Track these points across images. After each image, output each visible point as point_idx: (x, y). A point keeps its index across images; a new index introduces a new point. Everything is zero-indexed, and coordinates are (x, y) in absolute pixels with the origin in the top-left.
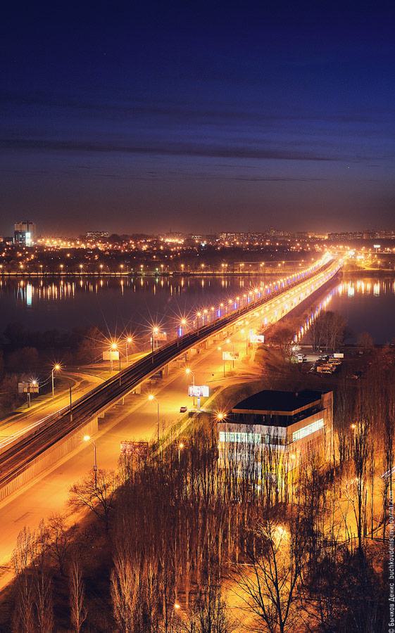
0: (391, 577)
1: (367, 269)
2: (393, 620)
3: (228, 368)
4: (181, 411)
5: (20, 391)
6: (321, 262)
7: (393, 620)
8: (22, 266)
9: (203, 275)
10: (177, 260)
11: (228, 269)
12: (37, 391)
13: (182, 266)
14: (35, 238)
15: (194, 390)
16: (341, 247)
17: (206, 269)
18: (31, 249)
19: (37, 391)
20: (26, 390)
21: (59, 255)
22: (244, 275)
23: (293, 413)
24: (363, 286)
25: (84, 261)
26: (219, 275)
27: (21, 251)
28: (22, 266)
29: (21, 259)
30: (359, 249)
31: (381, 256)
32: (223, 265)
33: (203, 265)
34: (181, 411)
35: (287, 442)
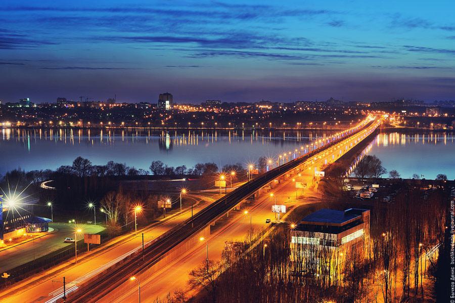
0: (452, 263)
1: (397, 127)
2: (453, 294)
3: (299, 193)
4: (267, 222)
5: (159, 207)
6: (364, 123)
7: (453, 294)
8: (163, 123)
9: (284, 130)
10: (267, 120)
11: (301, 126)
12: (170, 206)
13: (270, 124)
14: (172, 104)
15: (275, 208)
16: (379, 112)
17: (286, 126)
18: (170, 112)
19: (170, 206)
20: (163, 206)
21: (189, 115)
22: (312, 130)
23: (342, 224)
24: (395, 137)
25: (205, 121)
26: (295, 130)
27: (164, 114)
28: (163, 123)
29: (163, 118)
30: (391, 113)
31: (406, 118)
32: (298, 124)
33: (284, 124)
34: (267, 222)
35: (338, 244)
